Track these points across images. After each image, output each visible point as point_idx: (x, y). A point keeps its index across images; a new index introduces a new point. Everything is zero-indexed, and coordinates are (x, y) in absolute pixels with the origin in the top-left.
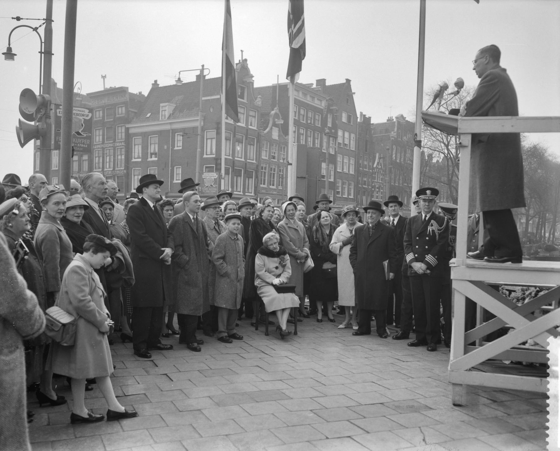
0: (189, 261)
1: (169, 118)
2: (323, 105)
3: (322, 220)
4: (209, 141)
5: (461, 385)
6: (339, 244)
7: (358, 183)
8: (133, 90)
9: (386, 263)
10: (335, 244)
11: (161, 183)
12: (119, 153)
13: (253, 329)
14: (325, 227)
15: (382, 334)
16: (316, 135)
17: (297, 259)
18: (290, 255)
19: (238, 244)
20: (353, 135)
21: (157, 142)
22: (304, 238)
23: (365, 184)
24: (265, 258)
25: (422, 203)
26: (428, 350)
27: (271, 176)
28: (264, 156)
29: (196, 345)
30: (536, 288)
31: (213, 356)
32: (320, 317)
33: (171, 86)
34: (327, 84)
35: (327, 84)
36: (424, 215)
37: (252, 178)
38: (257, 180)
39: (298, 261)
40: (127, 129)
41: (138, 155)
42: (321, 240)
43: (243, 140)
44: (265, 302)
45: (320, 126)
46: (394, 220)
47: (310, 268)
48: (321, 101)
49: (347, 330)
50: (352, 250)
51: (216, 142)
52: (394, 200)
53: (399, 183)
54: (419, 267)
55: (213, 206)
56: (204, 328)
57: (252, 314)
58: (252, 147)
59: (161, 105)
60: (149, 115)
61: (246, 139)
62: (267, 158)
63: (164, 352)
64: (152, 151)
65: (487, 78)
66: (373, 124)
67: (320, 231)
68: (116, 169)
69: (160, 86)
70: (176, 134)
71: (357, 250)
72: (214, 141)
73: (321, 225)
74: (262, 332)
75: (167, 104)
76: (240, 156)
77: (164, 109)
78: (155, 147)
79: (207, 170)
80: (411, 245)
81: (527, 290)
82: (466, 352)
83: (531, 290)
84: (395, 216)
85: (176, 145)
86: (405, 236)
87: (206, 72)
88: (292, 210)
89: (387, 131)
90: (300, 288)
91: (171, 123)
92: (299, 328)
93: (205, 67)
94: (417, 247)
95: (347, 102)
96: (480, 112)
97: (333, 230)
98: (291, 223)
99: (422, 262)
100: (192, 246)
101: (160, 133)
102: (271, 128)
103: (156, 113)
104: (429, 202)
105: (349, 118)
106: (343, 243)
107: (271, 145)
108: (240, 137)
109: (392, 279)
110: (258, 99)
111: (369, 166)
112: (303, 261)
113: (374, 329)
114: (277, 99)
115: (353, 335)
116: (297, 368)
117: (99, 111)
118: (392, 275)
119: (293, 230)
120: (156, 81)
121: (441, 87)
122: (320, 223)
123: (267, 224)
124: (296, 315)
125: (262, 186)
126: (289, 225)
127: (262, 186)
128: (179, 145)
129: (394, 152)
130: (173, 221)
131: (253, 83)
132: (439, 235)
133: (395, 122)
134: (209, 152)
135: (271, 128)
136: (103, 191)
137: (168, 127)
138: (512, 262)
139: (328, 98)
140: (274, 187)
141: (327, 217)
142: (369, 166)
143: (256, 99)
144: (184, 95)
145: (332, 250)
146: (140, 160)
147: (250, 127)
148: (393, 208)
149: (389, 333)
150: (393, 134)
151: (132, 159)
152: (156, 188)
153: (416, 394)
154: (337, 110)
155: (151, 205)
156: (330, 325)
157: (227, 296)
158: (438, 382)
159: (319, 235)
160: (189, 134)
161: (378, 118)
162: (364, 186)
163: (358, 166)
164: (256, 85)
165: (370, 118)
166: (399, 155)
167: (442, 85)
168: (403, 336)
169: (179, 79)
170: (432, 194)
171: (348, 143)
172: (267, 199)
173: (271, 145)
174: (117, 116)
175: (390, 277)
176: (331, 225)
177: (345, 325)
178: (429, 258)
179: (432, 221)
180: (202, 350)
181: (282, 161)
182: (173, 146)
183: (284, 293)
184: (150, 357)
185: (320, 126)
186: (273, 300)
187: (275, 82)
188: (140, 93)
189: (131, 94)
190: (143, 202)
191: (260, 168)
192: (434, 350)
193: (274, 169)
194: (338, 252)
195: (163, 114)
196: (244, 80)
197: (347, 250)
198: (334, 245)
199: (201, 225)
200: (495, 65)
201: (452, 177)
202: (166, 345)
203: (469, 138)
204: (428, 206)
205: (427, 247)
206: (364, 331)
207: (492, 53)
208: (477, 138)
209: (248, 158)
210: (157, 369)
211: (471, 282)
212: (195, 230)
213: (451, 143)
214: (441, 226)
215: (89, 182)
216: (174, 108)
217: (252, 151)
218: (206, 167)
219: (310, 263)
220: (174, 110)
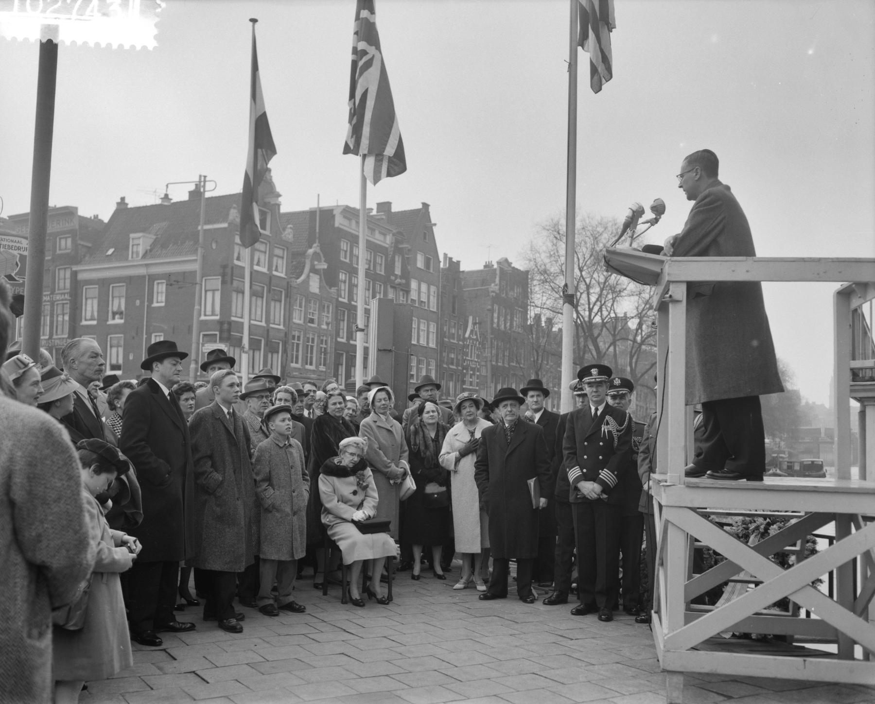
0: (222, 482)
1: (144, 256)
2: (387, 241)
3: (425, 416)
4: (210, 294)
5: (681, 673)
6: (454, 455)
7: (442, 361)
8: (85, 212)
9: (532, 482)
10: (448, 454)
11: (183, 356)
12: (59, 312)
13: (320, 593)
14: (428, 427)
15: (525, 597)
16: (378, 287)
17: (389, 478)
18: (375, 471)
19: (291, 453)
20: (433, 289)
21: (124, 294)
22: (402, 445)
23: (452, 364)
24: (335, 479)
25: (587, 390)
26: (600, 619)
27: (308, 349)
28: (297, 319)
29: (233, 622)
30: (765, 519)
31: (262, 640)
32: (417, 571)
33: (146, 207)
34: (393, 210)
35: (393, 210)
36: (593, 409)
37: (278, 352)
38: (285, 356)
39: (392, 482)
40: (74, 274)
41: (92, 315)
42: (422, 448)
43: (263, 294)
44: (341, 548)
45: (383, 273)
46: (597, 409)
47: (410, 492)
48: (385, 235)
49: (468, 592)
50: (478, 465)
51: (221, 298)
52: (537, 386)
53: (503, 363)
54: (590, 489)
55: (257, 395)
56: (234, 597)
57: (322, 570)
58: (278, 304)
59: (132, 236)
60: (110, 252)
61: (269, 291)
62: (301, 322)
63: (183, 635)
64: (115, 309)
65: (706, 200)
66: (463, 272)
67: (421, 433)
68: (55, 337)
69: (129, 206)
70: (156, 282)
71: (487, 465)
72: (218, 295)
73: (422, 425)
74: (336, 597)
75: (140, 235)
76: (258, 318)
77: (136, 242)
78: (120, 303)
79: (205, 339)
80: (575, 454)
81: (751, 523)
82: (687, 621)
83: (758, 523)
84: (537, 411)
85: (155, 300)
86: (564, 442)
87: (209, 186)
88: (384, 399)
89: (484, 282)
90: (394, 526)
91: (147, 265)
92: (395, 590)
93: (207, 179)
94: (585, 457)
95: (425, 238)
96: (696, 250)
97: (441, 433)
98: (381, 421)
99: (594, 480)
100: (228, 458)
101: (129, 280)
102: (308, 276)
103: (122, 249)
104: (597, 387)
105: (427, 262)
106: (460, 453)
107: (308, 301)
108: (259, 289)
109: (543, 508)
110: (288, 231)
111: (459, 336)
112: (399, 481)
113: (512, 587)
114: (317, 231)
115: (481, 599)
116: (409, 655)
117: (66, 238)
118: (543, 501)
119: (385, 432)
120: (123, 199)
121: (634, 212)
122: (421, 420)
123: (339, 424)
124: (396, 569)
125: (293, 365)
126: (378, 424)
127: (293, 365)
128: (160, 300)
129: (496, 315)
130: (196, 417)
131: (279, 205)
132: (619, 438)
133: (495, 270)
134: (209, 312)
135: (308, 276)
136: (97, 367)
137: (142, 271)
138: (748, 480)
139: (395, 231)
140: (313, 368)
141: (433, 411)
142: (459, 336)
143: (284, 229)
144: (176, 221)
145: (444, 465)
146: (95, 323)
147: (275, 273)
148: (535, 399)
149: (536, 596)
150: (494, 287)
151: (81, 321)
152: (175, 365)
153: (607, 690)
154: (409, 250)
155: (166, 392)
156: (438, 584)
157: (286, 542)
158: (633, 669)
159: (419, 440)
160: (181, 284)
161: (470, 264)
162: (451, 367)
163: (441, 335)
164: (284, 209)
165: (458, 262)
166: (502, 319)
167: (634, 209)
168: (560, 600)
169: (166, 196)
170: (600, 374)
171: (426, 301)
172: (330, 383)
173: (308, 301)
174: (58, 252)
175: (541, 504)
176: (438, 424)
177: (464, 583)
178: (605, 474)
179: (608, 417)
180: (245, 630)
181: (324, 327)
182: (151, 301)
183: (372, 533)
184: (160, 644)
185: (383, 273)
186: (354, 545)
187: (315, 206)
188: (96, 217)
189: (82, 219)
190: (153, 386)
191: (291, 337)
192: (609, 619)
193: (313, 339)
194: (452, 467)
195: (135, 250)
196: (267, 200)
197: (469, 464)
198: (446, 457)
199: (240, 423)
200: (711, 180)
201: (584, 353)
202: (183, 623)
203: (684, 288)
204: (596, 392)
205: (601, 457)
206: (497, 591)
207: (704, 164)
208: (695, 290)
209: (272, 321)
210: (175, 663)
211: (693, 509)
212: (232, 432)
213: (582, 301)
214: (621, 425)
215: (74, 353)
216: (152, 241)
217: (278, 311)
218: (204, 335)
219: (410, 484)
220: (154, 245)
